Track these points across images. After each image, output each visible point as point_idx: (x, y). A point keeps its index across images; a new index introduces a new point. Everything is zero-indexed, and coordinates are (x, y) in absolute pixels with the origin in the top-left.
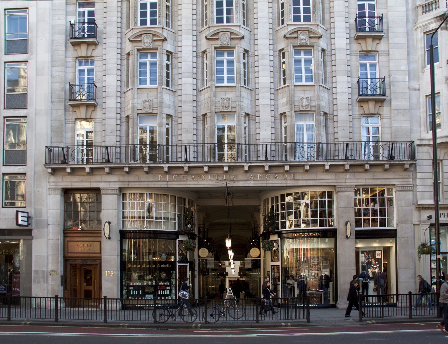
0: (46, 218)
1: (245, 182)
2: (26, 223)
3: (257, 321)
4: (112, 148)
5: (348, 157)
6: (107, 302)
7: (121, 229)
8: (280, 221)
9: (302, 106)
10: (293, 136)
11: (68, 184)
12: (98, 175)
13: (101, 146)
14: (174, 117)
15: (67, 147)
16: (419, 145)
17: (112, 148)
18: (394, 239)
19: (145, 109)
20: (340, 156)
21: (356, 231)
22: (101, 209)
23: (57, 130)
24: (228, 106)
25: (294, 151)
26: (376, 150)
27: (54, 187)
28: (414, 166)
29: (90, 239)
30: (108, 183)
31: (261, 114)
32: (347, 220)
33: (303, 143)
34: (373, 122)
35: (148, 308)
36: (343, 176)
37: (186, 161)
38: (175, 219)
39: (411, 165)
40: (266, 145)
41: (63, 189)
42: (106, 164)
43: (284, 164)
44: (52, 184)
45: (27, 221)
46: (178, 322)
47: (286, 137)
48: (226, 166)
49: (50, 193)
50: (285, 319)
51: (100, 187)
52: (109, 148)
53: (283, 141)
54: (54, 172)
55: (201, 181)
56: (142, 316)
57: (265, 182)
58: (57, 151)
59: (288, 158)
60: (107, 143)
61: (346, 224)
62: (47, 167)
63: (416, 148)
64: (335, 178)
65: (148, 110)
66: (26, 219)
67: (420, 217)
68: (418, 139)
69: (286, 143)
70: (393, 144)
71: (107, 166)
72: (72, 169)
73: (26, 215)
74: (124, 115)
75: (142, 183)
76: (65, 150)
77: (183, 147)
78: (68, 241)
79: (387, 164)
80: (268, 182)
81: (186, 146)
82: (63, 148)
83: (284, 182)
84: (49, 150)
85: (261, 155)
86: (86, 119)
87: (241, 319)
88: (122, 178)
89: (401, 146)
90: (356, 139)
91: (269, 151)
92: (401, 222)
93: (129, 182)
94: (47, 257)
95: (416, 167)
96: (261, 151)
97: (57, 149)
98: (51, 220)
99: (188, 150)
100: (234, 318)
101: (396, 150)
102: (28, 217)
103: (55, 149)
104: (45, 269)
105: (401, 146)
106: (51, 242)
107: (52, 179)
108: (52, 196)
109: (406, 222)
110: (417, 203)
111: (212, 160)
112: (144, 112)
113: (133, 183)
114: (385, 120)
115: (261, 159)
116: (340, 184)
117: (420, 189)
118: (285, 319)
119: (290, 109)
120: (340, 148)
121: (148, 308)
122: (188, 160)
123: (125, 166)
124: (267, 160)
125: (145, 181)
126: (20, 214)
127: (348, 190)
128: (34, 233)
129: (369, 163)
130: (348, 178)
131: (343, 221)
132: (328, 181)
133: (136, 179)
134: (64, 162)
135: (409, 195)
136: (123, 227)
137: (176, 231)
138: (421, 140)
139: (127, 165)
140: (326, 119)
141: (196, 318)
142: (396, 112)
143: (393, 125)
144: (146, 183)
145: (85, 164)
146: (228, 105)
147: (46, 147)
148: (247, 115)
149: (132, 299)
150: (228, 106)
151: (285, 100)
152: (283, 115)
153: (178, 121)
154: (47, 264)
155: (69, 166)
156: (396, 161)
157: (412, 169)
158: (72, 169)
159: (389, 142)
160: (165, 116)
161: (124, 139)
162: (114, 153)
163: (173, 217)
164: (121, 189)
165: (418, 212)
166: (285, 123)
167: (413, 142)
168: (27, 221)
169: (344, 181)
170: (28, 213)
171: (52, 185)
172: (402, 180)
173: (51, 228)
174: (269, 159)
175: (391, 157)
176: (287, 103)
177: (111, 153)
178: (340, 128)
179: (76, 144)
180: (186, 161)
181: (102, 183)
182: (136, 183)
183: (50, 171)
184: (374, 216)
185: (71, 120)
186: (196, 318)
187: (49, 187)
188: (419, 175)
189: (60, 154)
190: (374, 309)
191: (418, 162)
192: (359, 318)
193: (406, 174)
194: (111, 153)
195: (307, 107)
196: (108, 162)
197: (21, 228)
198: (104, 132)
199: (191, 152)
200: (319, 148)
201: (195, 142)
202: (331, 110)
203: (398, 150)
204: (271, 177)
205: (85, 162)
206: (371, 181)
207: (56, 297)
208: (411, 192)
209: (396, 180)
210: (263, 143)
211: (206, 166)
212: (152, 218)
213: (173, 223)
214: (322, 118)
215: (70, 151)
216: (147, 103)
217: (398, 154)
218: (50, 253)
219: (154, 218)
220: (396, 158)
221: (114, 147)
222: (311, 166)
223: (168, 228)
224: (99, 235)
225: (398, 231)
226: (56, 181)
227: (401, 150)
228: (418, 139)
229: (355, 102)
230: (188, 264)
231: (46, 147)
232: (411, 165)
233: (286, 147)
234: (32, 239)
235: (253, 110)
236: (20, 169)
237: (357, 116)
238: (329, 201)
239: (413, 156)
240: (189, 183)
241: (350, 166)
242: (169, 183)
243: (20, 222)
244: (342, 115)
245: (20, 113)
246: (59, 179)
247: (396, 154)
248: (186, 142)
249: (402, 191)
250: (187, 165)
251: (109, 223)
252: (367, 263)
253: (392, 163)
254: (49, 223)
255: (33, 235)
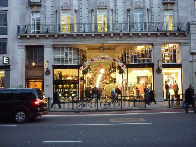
0: (17, 60)
1: (111, 41)
2: (7, 63)
3: (145, 107)
4: (49, 25)
5: (159, 30)
6: (50, 100)
7: (53, 64)
8: (79, 60)
9: (137, 6)
10: (133, 20)
11: (28, 43)
12: (51, 38)
13: (44, 25)
14: (78, 11)
15: (28, 25)
16: (192, 24)
17: (49, 25)
18: (180, 68)
19: (65, 7)
20: (155, 29)
21: (163, 64)
22: (44, 55)
23: (23, 18)
24: (103, 6)
25: (133, 27)
26: (38, 28)
27: (21, 45)
28: (189, 34)
29: (38, 70)
30: (47, 43)
31: (118, 9)
32: (158, 59)
33: (137, 23)
34: (36, 16)
35: (70, 102)
36: (156, 38)
37: (84, 32)
38: (78, 59)
39: (188, 33)
40: (121, 24)
41: (25, 45)
42: (46, 34)
43: (129, 33)
44: (20, 43)
45: (8, 62)
46: (87, 109)
47: (129, 20)
48: (103, 34)
49: (19, 48)
50: (134, 106)
51: (44, 44)
52: (48, 26)
53: (128, 22)
54: (22, 37)
55: (91, 41)
56: (67, 106)
57: (121, 41)
58: (23, 27)
59: (131, 30)
60: (47, 23)
61: (158, 61)
62: (18, 35)
63: (190, 25)
64: (170, 39)
65: (66, 7)
66: (7, 61)
67: (193, 57)
68: (191, 21)
69: (129, 23)
70: (179, 23)
71: (47, 34)
72: (30, 36)
73: (7, 59)
74: (54, 10)
75: (63, 42)
76: (26, 27)
77: (83, 25)
78: (28, 71)
79: (177, 33)
80: (122, 41)
81: (84, 25)
82: (26, 26)
83: (129, 41)
84: (19, 27)
85: (119, 29)
86: (37, 12)
87: (118, 107)
88: (54, 40)
89: (184, 24)
90: (162, 21)
91: (122, 27)
92: (184, 60)
93: (57, 42)
94: (18, 79)
95: (190, 34)
96: (119, 27)
97: (23, 26)
98: (19, 61)
99: (85, 26)
100: (114, 106)
101: (181, 26)
102: (9, 60)
103: (22, 26)
104: (16, 85)
105: (183, 24)
106: (19, 71)
107: (20, 41)
108: (20, 49)
109: (186, 60)
110: (191, 51)
111: (96, 31)
112: (64, 8)
113: (59, 42)
114: (175, 12)
115: (119, 31)
116: (155, 42)
117: (192, 45)
118: (134, 106)
119: (132, 7)
120: (155, 26)
121: (70, 102)
122: (85, 31)
123: (55, 34)
124: (121, 31)
125: (65, 42)
126: (5, 58)
127: (159, 45)
128: (11, 67)
129: (169, 32)
130: (159, 39)
131: (156, 60)
132: (149, 41)
133: (61, 41)
134: (26, 33)
135: (187, 48)
136: (54, 64)
137: (79, 65)
138: (192, 21)
139: (56, 34)
140: (148, 12)
141: (108, 106)
142: (180, 8)
143: (179, 15)
144: (65, 42)
145: (36, 34)
146: (103, 5)
147: (18, 25)
148: (112, 10)
149: (63, 98)
150: (103, 6)
151: (129, 3)
152: (128, 10)
153: (80, 13)
154: (18, 82)
155: (29, 35)
156: (181, 31)
157: (188, 35)
158: (30, 36)
159: (178, 22)
160: (74, 10)
161: (54, 22)
162: (50, 28)
163: (77, 58)
164: (53, 46)
165: (192, 56)
166: (129, 14)
167: (189, 22)
168: (8, 62)
169: (157, 41)
170: (8, 58)
171: (20, 44)
172: (185, 40)
173: (19, 65)
174: (123, 31)
175: (179, 30)
176: (130, 4)
177: (49, 28)
178: (82, 17)
179: (31, 24)
180: (84, 32)
181: (45, 43)
182: (61, 42)
183: (19, 37)
184: (143, 58)
185: (29, 12)
186: (108, 106)
187: (19, 45)
188: (192, 38)
189: (24, 29)
190: (172, 102)
191: (191, 32)
192: (169, 106)
193: (186, 37)
194: (49, 28)
195: (139, 6)
196: (47, 32)
197: (5, 65)
198: (45, 18)
199: (86, 27)
200: (145, 25)
201: (88, 23)
202: (150, 7)
203: (182, 26)
204: (123, 39)
205: (36, 32)
206: (169, 41)
207: (49, 98)
208: (188, 46)
209: (181, 41)
210: (119, 23)
211: (93, 34)
212: (68, 59)
213: (77, 62)
214: (146, 11)
215: (29, 27)
216: (66, 4)
217: (182, 28)
218: (19, 77)
219: (65, 59)
220: (181, 30)
221: (86, 25)
222: (114, 34)
223: (75, 63)
224: (43, 68)
225: (182, 65)
226: (22, 42)
227: (183, 26)
228: (191, 21)
229: (161, 4)
230: (84, 81)
231: (18, 25)
232: (188, 33)
233: (129, 25)
234: (10, 70)
235: (115, 8)
236: (4, 36)
237: (162, 10)
238: (149, 50)
239: (189, 29)
240: (85, 42)
241: (178, 34)
242: (76, 42)
243: (5, 62)
244: (156, 10)
245: (5, 9)
246: (24, 41)
247: (181, 28)
248: (84, 23)
249: (184, 45)
250: (85, 33)
251: (48, 62)
252: (168, 80)
253: (179, 32)
254: (19, 62)
255: (11, 68)
